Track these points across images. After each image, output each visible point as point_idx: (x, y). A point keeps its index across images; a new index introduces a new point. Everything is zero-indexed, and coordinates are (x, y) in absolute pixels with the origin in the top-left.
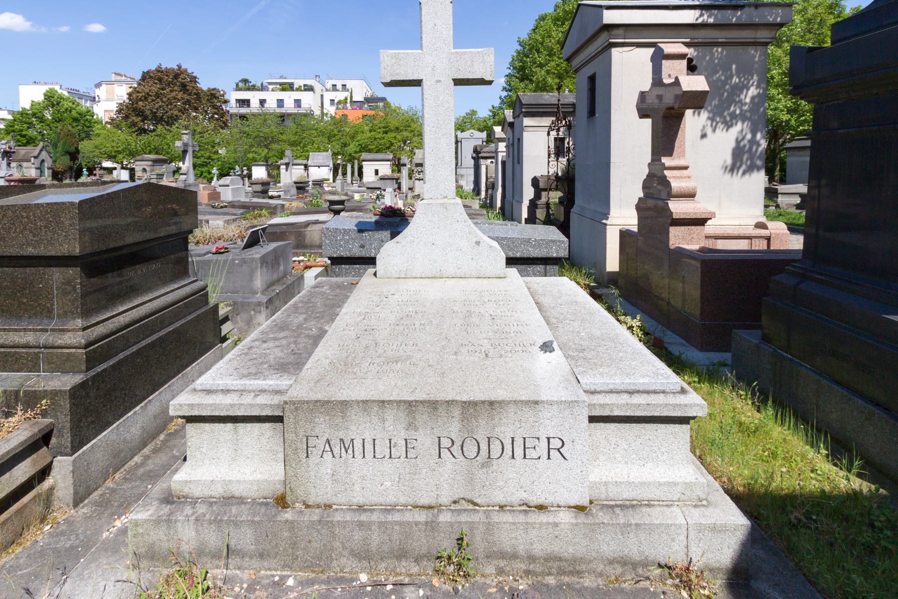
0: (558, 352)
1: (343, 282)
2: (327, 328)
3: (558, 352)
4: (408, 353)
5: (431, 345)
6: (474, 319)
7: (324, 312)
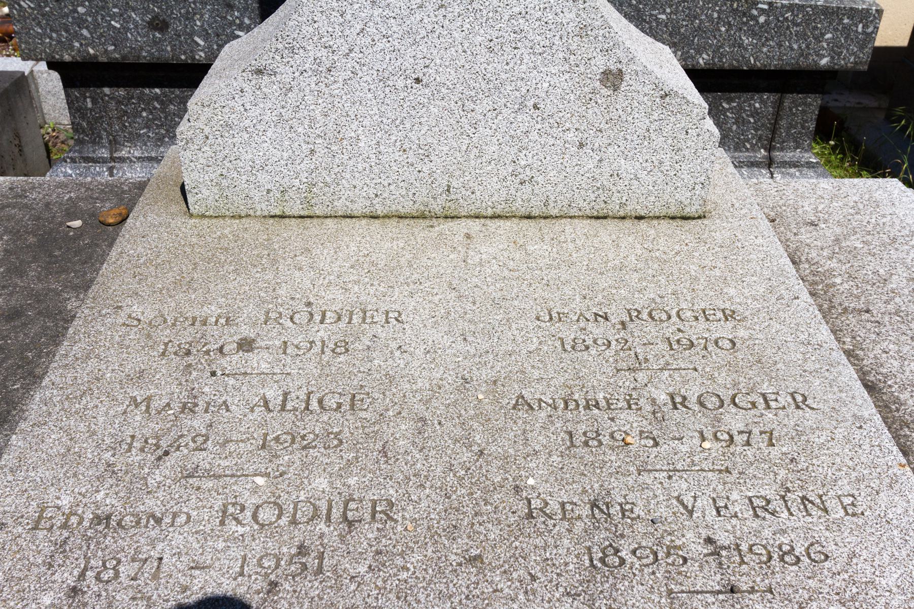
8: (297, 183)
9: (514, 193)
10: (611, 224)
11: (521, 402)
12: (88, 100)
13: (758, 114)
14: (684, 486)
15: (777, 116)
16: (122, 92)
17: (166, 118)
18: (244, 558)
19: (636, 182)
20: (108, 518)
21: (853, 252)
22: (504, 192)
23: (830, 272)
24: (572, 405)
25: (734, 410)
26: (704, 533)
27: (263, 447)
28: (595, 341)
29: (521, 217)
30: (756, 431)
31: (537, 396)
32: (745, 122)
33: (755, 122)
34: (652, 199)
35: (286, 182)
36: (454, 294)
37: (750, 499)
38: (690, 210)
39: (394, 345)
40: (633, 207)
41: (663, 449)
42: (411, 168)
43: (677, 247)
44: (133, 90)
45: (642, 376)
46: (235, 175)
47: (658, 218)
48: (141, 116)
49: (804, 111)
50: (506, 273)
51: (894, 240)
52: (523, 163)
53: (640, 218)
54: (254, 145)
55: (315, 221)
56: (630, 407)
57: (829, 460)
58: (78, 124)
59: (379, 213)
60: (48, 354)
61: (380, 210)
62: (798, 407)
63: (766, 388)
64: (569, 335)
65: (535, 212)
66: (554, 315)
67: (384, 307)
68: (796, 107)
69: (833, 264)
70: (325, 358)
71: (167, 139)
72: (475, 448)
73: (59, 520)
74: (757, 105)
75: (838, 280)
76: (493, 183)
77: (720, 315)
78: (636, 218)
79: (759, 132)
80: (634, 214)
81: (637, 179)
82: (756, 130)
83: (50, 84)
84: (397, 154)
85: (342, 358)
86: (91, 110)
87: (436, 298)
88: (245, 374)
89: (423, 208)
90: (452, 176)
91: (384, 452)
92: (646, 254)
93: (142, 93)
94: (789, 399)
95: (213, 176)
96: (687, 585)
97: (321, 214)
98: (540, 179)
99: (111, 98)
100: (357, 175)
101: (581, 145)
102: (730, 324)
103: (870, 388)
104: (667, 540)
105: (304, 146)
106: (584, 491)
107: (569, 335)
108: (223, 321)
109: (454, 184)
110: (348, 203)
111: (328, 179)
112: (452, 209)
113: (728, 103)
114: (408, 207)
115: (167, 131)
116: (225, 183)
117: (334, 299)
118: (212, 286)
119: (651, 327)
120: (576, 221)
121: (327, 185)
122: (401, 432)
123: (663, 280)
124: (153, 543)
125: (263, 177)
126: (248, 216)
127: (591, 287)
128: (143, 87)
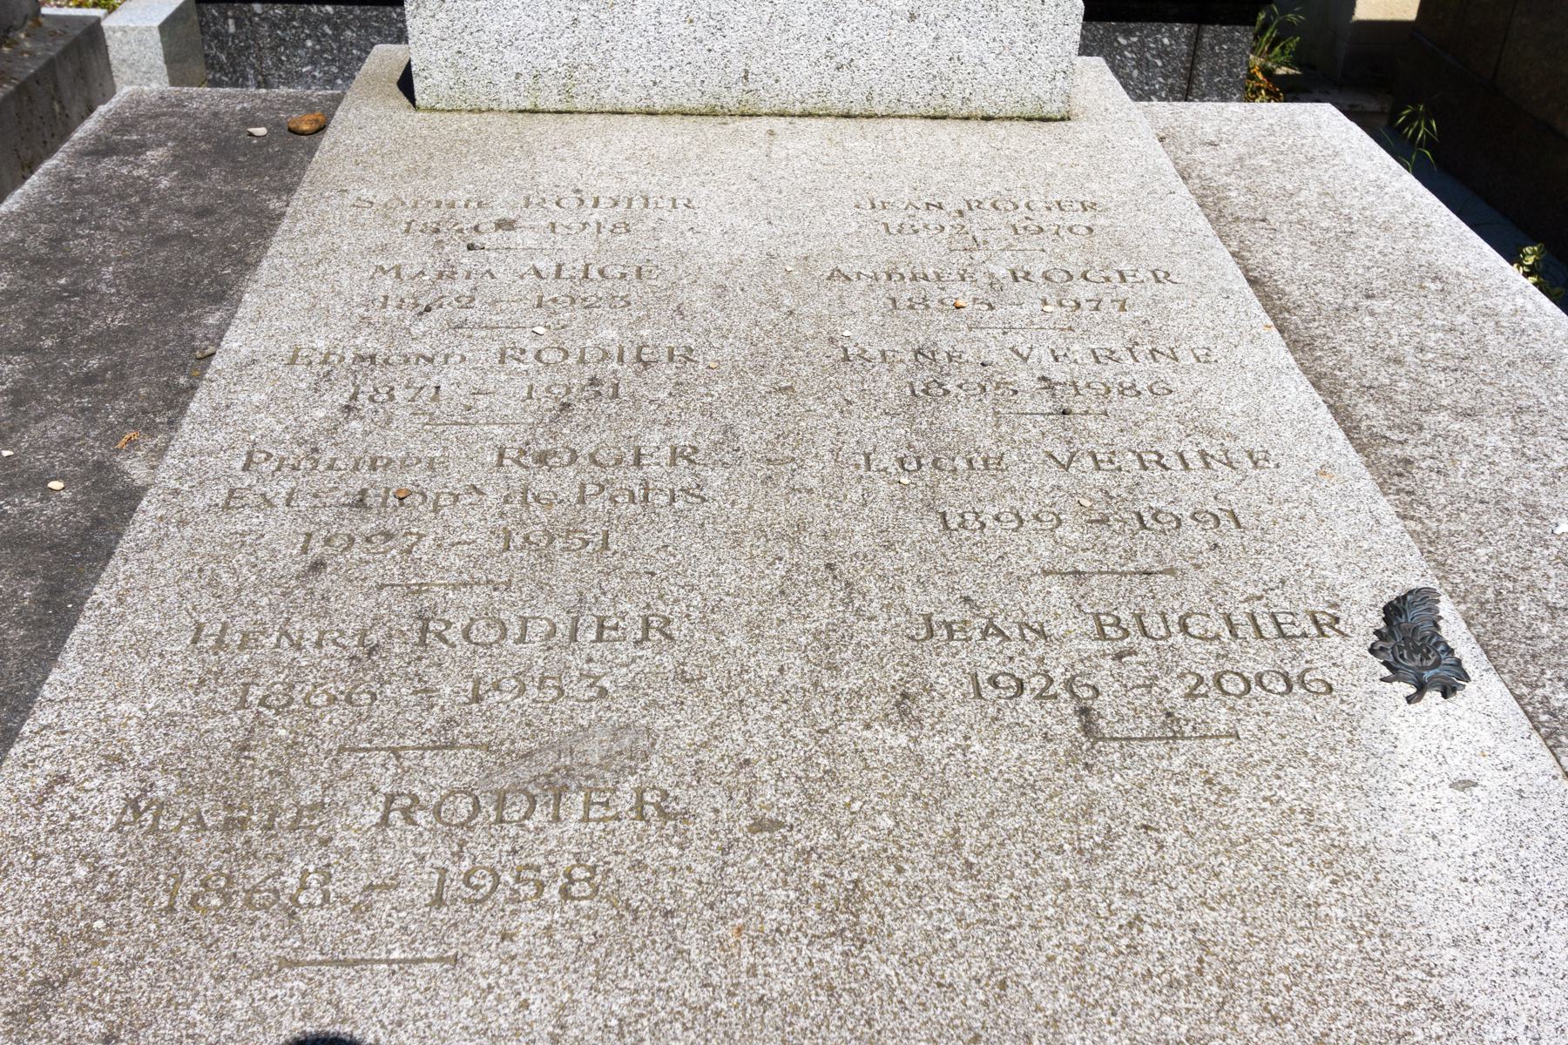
0: (1486, 689)
1: (249, 119)
2: (136, 469)
3: (1486, 689)
4: (627, 708)
5: (754, 630)
6: (964, 417)
7: (129, 334)
8: (554, 64)
9: (828, 81)
10: (951, 127)
11: (836, 274)
12: (231, 21)
13: (1167, 54)
14: (1020, 339)
15: (1194, 57)
16: (279, 10)
17: (339, 49)
18: (531, 387)
19: (981, 69)
20: (373, 357)
21: (1259, 170)
22: (815, 80)
23: (1226, 187)
24: (896, 277)
25: (1084, 283)
26: (1038, 374)
27: (539, 306)
28: (926, 226)
29: (838, 116)
30: (1107, 299)
31: (857, 269)
32: (1150, 65)
33: (1164, 66)
34: (1003, 92)
35: (541, 63)
36: (755, 184)
37: (1093, 352)
38: (1051, 109)
39: (685, 227)
40: (978, 104)
41: (999, 312)
42: (700, 46)
43: (1032, 147)
44: (294, 7)
45: (978, 256)
46: (476, 53)
47: (1011, 119)
48: (304, 46)
49: (1230, 52)
50: (819, 166)
51: (1313, 159)
52: (840, 40)
53: (987, 119)
54: (502, 11)
55: (576, 116)
56: (963, 279)
57: (1187, 323)
58: (215, 57)
59: (657, 107)
60: (257, 246)
61: (659, 104)
62: (1158, 281)
63: (1123, 266)
64: (894, 221)
65: (856, 110)
66: (877, 203)
67: (669, 195)
68: (1220, 44)
69: (1232, 179)
70: (603, 237)
71: (339, 82)
72: (785, 309)
73: (317, 358)
74: (1166, 41)
75: (1233, 194)
76: (803, 68)
77: (1077, 206)
78: (983, 118)
79: (1170, 81)
80: (980, 114)
81: (983, 64)
82: (1165, 77)
83: (126, 48)
84: (682, 25)
85: (623, 237)
86: (234, 36)
87: (734, 188)
88: (508, 249)
89: (713, 102)
90: (750, 57)
91: (679, 310)
92: (993, 152)
93: (308, 12)
94: (1150, 275)
95: (448, 54)
96: (1015, 408)
97: (583, 109)
98: (861, 63)
99: (263, 20)
100: (631, 54)
101: (912, 17)
102: (1089, 214)
103: (1253, 282)
104: (998, 378)
105: (566, 14)
106: (908, 342)
107: (894, 221)
108: (474, 204)
109: (753, 69)
110: (618, 94)
111: (594, 60)
112: (751, 104)
113: (1126, 38)
114: (694, 101)
115: (341, 69)
116: (463, 63)
117: (608, 187)
118: (455, 174)
119: (995, 217)
120: (907, 121)
121: (592, 67)
122: (699, 299)
123: (1012, 175)
124: (427, 376)
125: (511, 56)
126: (490, 110)
127: (924, 180)
128: (309, 3)
